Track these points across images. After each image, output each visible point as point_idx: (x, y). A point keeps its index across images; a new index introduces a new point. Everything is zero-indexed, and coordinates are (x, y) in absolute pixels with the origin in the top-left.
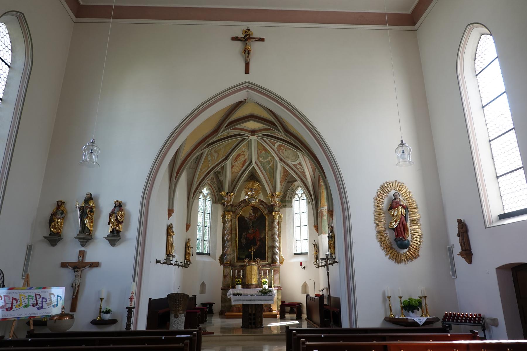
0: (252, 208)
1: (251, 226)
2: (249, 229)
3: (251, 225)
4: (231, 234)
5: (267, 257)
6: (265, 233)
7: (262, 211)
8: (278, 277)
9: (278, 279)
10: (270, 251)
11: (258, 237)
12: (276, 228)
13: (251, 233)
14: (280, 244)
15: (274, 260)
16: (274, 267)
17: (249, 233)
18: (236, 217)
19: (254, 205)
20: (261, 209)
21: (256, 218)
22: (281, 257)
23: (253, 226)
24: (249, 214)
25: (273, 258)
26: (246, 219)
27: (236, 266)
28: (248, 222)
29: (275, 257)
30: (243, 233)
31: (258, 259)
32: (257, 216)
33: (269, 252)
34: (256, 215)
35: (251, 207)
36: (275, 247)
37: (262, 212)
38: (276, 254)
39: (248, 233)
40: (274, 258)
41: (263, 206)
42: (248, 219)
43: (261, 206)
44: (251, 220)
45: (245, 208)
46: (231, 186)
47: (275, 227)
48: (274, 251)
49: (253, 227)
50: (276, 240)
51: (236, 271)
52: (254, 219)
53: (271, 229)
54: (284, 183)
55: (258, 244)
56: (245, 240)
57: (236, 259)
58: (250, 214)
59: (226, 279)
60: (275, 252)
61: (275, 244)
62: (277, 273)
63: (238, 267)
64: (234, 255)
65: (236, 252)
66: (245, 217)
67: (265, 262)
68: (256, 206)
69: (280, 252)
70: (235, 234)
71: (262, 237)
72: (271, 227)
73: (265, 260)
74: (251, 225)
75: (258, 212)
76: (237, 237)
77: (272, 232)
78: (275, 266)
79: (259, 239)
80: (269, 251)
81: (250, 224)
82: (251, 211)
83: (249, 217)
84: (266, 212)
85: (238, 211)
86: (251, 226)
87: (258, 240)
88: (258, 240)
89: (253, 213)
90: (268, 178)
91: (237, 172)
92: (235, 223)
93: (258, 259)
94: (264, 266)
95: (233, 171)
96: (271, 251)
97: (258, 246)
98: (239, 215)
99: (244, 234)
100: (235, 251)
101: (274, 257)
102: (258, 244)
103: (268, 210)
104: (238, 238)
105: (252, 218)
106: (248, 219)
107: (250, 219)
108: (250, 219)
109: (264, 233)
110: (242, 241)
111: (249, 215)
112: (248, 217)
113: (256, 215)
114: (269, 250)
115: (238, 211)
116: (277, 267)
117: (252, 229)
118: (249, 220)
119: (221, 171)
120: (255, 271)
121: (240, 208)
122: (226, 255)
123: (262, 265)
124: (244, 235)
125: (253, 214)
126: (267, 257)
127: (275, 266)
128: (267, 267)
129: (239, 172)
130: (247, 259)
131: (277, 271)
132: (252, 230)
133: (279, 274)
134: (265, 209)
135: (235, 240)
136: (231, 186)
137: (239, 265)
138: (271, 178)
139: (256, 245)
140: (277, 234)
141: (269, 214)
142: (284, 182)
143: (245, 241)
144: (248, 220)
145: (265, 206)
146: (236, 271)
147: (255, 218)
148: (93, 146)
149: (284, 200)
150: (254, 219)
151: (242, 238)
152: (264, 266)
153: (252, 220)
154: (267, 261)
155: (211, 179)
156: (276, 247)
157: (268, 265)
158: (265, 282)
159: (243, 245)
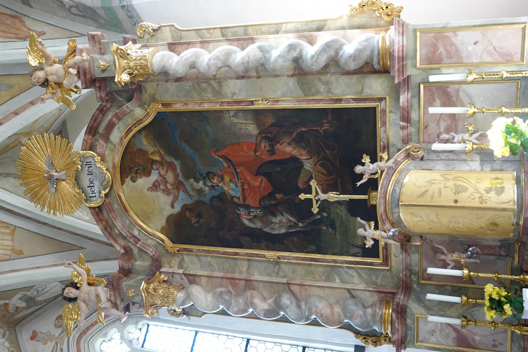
0: (128, 180)
1: (209, 184)
2: (222, 197)
3: (201, 183)
4: (249, 284)
5: (355, 100)
6: (235, 116)
7: (135, 130)
8: (476, 35)
9: (490, 32)
10: (327, 83)
11: (255, 151)
12: (197, 56)
13: (239, 185)
14: (286, 32)
15: (367, 64)
16: (409, 63)
17: (239, 195)
18: (173, 255)
19: (114, 167)
20: (127, 133)
21: (169, 159)
22: (357, 21)
23: (208, 174)
24: (154, 194)
25: (362, 67)
26: (177, 208)
27: (408, 269)
28: (189, 201)
29: (354, 57)
30: (243, 224)
31: (359, 169)
32: (161, 156)
33: (329, 91)
34: (157, 158)
35: (123, 182)
36: (297, 61)
37: (140, 131)
38: (337, 52)
39: (241, 202)
40: (361, 62)
41: (111, 127)
42: (176, 199)
43: (116, 136)
44: (179, 185)
45: (132, 213)
46: (83, 248)
47: (193, 66)
48: (317, 67)
49: (209, 175)
50: (259, 54)
51: (431, 270)
52: (174, 169)
53: (213, 82)
54: (29, 23)
55: (289, 149)
56: (276, 216)
57: (371, 264)
58: (155, 187)
59: (477, 338)
60: (323, 60)
61: (276, 60)
62: (452, 44)
63: (415, 257)
64: (351, 272)
65: (335, 261)
66: (168, 211)
67: (384, 111)
68: (118, 159)
69: (329, 24)
70: (249, 260)
71: (252, 129)
72: (204, 85)
73: (374, 109)
74: (201, 183)
75: (142, 152)
76: (264, 256)
77: (226, 78)
78: (402, 59)
79: (264, 145)
80: (322, 88)
81: (200, 192)
82: (144, 183)
83: (167, 192)
84: (139, 112)
85: (149, 241)
86: (205, 184)
87: (272, 151)
88: (272, 151)
89: (148, 174)
90: (17, 98)
91: (12, 234)
92: (202, 258)
93: (359, 169)
94: (406, 118)
95: (9, 252)
96: (324, 78)
97: (303, 152)
98: (163, 241)
99: (246, 222)
100: (331, 266)
101: (352, 66)
102: (289, 149)
103: (129, 100)
104: (269, 249)
105: (170, 177)
106: (176, 199)
107: (178, 189)
108: (178, 189)
109: (235, 120)
110: (283, 231)
111: (160, 194)
112: (170, 199)
113: (153, 162)
114: (318, 92)
115: (149, 241)
116: (411, 46)
117: (222, 179)
118: (182, 195)
119: (19, 296)
120: (434, 188)
121: (136, 233)
122: (346, 321)
123: (403, 128)
124: (250, 220)
125: (154, 177)
126: (355, 100)
127: (402, 59)
128: (415, 101)
129: (7, 225)
130: (361, 231)
131: (435, 46)
132: (227, 178)
133: (456, 30)
134: (125, 114)
135: (277, 262)
136: (83, 248)
137: (402, 257)
138: (11, 87)
139: (295, 160)
140: (228, 54)
141: (146, 96)
142: (22, 21)
143: (279, 218)
144: (183, 199)
145: (109, 116)
146: (431, 270)
147: (171, 166)
148: (251, 263)
149: (101, 12)
150: (174, 169)
151: (266, 230)
152: (406, 118)
153: (181, 178)
154: (381, 100)
155: (60, 326)
156: (295, 54)
157: (403, 98)
158: (513, 141)
159: (300, 225)
